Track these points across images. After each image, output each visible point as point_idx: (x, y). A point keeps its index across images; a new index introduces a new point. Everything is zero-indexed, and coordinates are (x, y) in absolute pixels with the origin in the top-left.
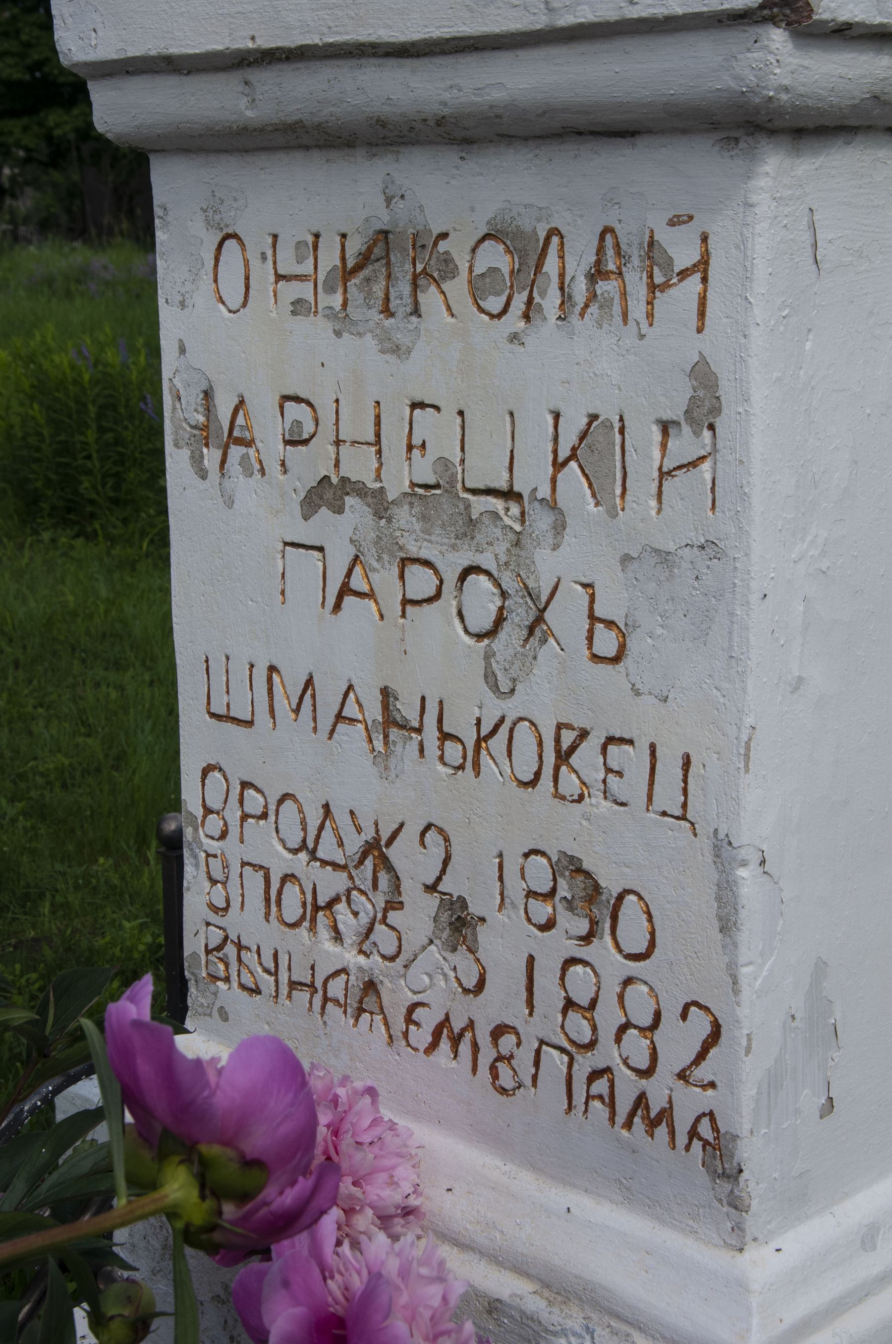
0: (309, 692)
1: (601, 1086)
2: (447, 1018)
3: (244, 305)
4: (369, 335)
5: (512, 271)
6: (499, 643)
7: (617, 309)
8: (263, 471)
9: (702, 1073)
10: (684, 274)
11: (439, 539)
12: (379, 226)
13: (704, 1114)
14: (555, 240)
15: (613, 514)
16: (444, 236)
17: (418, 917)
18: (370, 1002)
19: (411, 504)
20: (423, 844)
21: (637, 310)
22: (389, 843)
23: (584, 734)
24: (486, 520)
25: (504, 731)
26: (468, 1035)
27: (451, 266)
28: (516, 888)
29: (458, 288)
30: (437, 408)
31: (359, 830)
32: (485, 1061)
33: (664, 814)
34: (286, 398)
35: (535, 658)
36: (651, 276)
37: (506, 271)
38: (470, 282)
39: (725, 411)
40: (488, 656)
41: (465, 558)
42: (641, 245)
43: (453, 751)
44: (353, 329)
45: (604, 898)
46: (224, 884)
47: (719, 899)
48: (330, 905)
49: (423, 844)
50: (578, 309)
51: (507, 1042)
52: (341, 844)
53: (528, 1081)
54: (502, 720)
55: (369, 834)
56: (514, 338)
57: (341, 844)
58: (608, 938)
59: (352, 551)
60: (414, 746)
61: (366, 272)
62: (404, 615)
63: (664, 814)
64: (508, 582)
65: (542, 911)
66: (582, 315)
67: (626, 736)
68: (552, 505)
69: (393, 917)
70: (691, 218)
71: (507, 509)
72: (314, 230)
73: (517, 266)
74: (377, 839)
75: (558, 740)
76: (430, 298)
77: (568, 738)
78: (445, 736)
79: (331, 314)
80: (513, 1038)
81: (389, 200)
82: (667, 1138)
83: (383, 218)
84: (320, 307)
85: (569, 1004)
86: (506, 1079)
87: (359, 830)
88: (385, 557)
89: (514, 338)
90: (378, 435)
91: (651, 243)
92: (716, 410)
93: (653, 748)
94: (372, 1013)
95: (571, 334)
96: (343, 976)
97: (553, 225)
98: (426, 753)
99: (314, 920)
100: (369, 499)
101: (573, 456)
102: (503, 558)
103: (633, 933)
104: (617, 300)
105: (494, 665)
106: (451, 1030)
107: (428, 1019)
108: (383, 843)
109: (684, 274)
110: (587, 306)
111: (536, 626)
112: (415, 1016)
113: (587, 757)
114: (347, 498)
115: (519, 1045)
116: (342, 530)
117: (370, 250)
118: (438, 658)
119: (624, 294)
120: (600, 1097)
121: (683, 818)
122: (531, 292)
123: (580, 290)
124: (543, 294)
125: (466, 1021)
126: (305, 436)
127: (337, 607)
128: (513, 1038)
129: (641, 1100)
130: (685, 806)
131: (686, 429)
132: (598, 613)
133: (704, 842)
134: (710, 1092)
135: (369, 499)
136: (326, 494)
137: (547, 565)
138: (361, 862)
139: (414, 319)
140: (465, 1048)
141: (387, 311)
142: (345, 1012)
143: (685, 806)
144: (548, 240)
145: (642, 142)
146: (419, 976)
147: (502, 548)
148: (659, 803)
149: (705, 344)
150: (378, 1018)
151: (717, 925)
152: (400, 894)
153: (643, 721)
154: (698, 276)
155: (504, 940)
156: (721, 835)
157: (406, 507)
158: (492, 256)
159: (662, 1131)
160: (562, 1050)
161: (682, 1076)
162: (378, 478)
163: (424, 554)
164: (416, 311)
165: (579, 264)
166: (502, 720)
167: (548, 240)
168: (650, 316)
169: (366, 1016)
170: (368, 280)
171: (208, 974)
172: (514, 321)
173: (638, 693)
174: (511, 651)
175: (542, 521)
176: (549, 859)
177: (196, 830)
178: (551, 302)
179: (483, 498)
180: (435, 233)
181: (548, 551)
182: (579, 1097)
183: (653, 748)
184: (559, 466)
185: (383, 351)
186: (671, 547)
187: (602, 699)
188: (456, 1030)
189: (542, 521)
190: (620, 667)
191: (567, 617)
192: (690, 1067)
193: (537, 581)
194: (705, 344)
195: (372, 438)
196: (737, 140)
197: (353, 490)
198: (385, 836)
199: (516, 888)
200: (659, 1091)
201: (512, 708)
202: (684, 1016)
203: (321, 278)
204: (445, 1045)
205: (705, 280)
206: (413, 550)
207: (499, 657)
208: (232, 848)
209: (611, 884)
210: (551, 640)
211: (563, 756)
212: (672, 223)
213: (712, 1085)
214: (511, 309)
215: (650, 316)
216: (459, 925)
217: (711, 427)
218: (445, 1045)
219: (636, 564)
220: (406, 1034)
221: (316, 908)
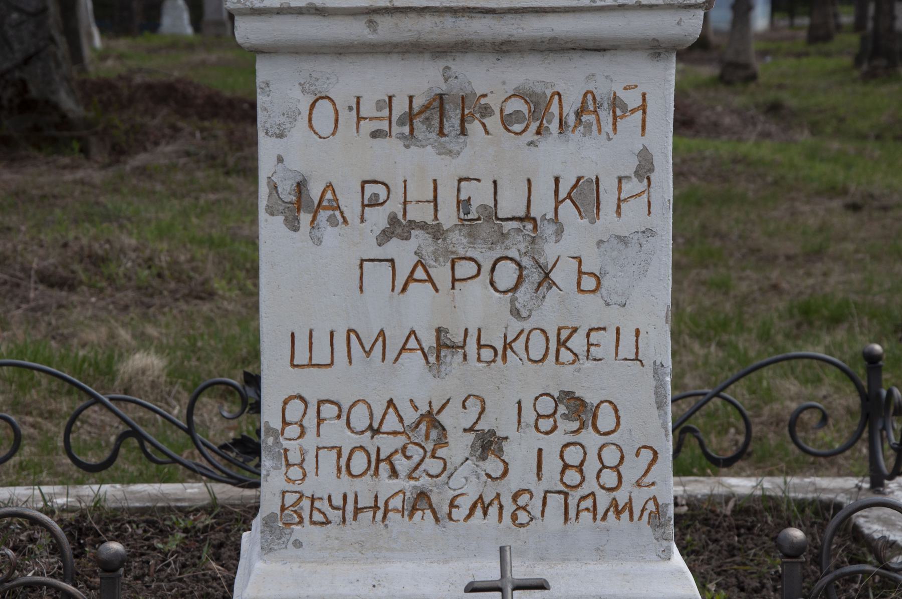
0: (381, 339)
1: (588, 503)
2: (481, 497)
3: (333, 134)
4: (429, 147)
5: (530, 111)
6: (520, 294)
7: (595, 127)
8: (345, 221)
9: (648, 480)
10: (633, 111)
11: (480, 246)
12: (439, 91)
13: (650, 499)
14: (353, 336)
15: (593, 222)
16: (484, 96)
17: (459, 446)
18: (423, 504)
19: (460, 230)
20: (464, 407)
21: (607, 127)
22: (439, 412)
23: (575, 330)
24: (512, 233)
25: (523, 338)
26: (496, 502)
27: (489, 110)
28: (529, 416)
29: (493, 122)
30: (479, 180)
31: (416, 408)
32: (507, 514)
33: (626, 359)
34: (365, 182)
35: (544, 297)
36: (614, 112)
37: (526, 112)
38: (502, 118)
39: (656, 169)
40: (513, 301)
41: (498, 252)
42: (609, 99)
43: (487, 354)
44: (418, 143)
45: (588, 408)
46: (301, 465)
47: (656, 393)
48: (389, 459)
49: (464, 407)
50: (571, 129)
51: (523, 500)
52: (401, 420)
53: (539, 515)
54: (522, 331)
55: (424, 409)
56: (531, 143)
57: (401, 420)
58: (590, 428)
59: (416, 258)
60: (460, 357)
61: (427, 114)
62: (453, 288)
63: (626, 359)
64: (526, 262)
65: (545, 424)
66: (573, 131)
67: (602, 326)
68: (556, 220)
69: (440, 453)
70: (636, 86)
71: (524, 227)
72: (390, 94)
73: (533, 109)
74: (429, 413)
75: (559, 334)
76: (474, 127)
77: (564, 334)
78: (480, 346)
79: (402, 137)
80: (527, 496)
81: (446, 80)
82: (628, 517)
83: (444, 88)
84: (393, 134)
85: (566, 466)
86: (523, 517)
87: (416, 408)
88: (441, 259)
89: (531, 143)
90: (435, 197)
91: (615, 98)
92: (652, 170)
93: (618, 330)
94: (423, 510)
95: (568, 141)
96: (401, 495)
97: (556, 90)
98: (468, 357)
99: (377, 468)
100: (430, 230)
101: (569, 196)
102: (523, 251)
103: (606, 420)
104: (595, 122)
105: (517, 304)
106: (483, 503)
107: (465, 504)
108: (435, 412)
109: (633, 111)
110: (575, 126)
111: (546, 279)
112: (456, 503)
113: (578, 343)
114: (412, 231)
115: (531, 498)
116: (404, 252)
117: (430, 103)
118: (478, 307)
119: (598, 121)
120: (587, 509)
121: (637, 359)
122: (542, 121)
123: (572, 120)
124: (549, 122)
125: (495, 495)
126: (381, 201)
127: (404, 289)
128: (527, 496)
129: (614, 503)
130: (637, 353)
131: (635, 180)
132: (584, 269)
133: (649, 369)
134: (652, 488)
135: (430, 230)
136: (397, 228)
137: (550, 251)
138: (417, 426)
139: (462, 138)
140: (493, 511)
141: (441, 133)
142: (403, 516)
143: (637, 353)
144: (552, 97)
145: (608, 53)
146: (457, 481)
147: (523, 247)
148: (621, 355)
149: (645, 141)
150: (428, 512)
151: (655, 406)
152: (446, 438)
153: (612, 317)
154: (641, 112)
155: (520, 451)
156: (658, 363)
157: (457, 232)
158: (517, 105)
159: (626, 515)
160: (559, 492)
161: (638, 484)
162: (436, 218)
163: (469, 254)
164: (463, 132)
165: (570, 111)
166: (522, 331)
167: (552, 97)
168: (615, 129)
169: (419, 513)
170: (427, 119)
171: (284, 524)
172: (530, 135)
173: (608, 305)
174: (529, 296)
175: (549, 230)
176: (552, 397)
177: (276, 438)
178: (554, 126)
179: (510, 223)
180: (478, 95)
181: (552, 244)
182: (572, 513)
183: (618, 330)
184: (558, 203)
185: (439, 154)
186: (627, 234)
187: (589, 311)
188: (487, 503)
189: (549, 230)
190: (598, 294)
191: (563, 275)
192: (641, 478)
193: (546, 258)
194: (645, 141)
195: (431, 197)
196: (659, 54)
197: (418, 227)
198: (436, 408)
199: (529, 416)
200: (622, 497)
201: (527, 325)
202: (637, 455)
203: (394, 118)
204: (479, 512)
205: (644, 112)
206: (462, 252)
207: (520, 300)
208: (310, 441)
209: (591, 399)
210: (554, 287)
211: (562, 344)
212: (625, 89)
213: (653, 484)
214: (529, 130)
215: (615, 129)
216: (488, 444)
217: (649, 179)
218: (479, 512)
219: (606, 244)
220: (450, 514)
221: (378, 460)
